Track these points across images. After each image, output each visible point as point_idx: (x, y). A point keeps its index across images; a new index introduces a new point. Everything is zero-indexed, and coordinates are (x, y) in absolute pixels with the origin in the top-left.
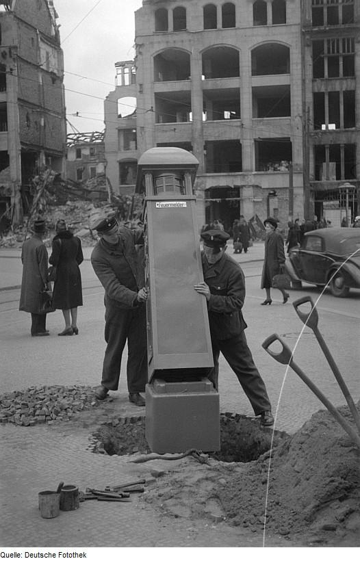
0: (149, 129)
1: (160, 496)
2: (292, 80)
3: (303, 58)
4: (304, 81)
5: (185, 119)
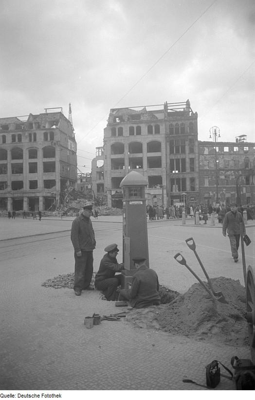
0: (109, 172)
1: (133, 318)
2: (162, 154)
3: (166, 146)
4: (166, 155)
5: (122, 168)
